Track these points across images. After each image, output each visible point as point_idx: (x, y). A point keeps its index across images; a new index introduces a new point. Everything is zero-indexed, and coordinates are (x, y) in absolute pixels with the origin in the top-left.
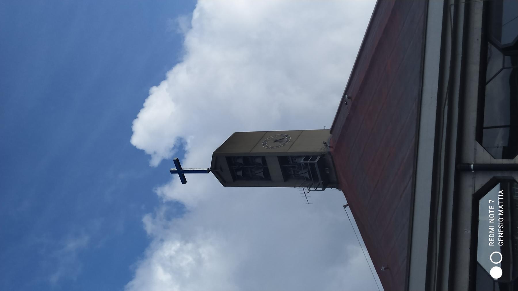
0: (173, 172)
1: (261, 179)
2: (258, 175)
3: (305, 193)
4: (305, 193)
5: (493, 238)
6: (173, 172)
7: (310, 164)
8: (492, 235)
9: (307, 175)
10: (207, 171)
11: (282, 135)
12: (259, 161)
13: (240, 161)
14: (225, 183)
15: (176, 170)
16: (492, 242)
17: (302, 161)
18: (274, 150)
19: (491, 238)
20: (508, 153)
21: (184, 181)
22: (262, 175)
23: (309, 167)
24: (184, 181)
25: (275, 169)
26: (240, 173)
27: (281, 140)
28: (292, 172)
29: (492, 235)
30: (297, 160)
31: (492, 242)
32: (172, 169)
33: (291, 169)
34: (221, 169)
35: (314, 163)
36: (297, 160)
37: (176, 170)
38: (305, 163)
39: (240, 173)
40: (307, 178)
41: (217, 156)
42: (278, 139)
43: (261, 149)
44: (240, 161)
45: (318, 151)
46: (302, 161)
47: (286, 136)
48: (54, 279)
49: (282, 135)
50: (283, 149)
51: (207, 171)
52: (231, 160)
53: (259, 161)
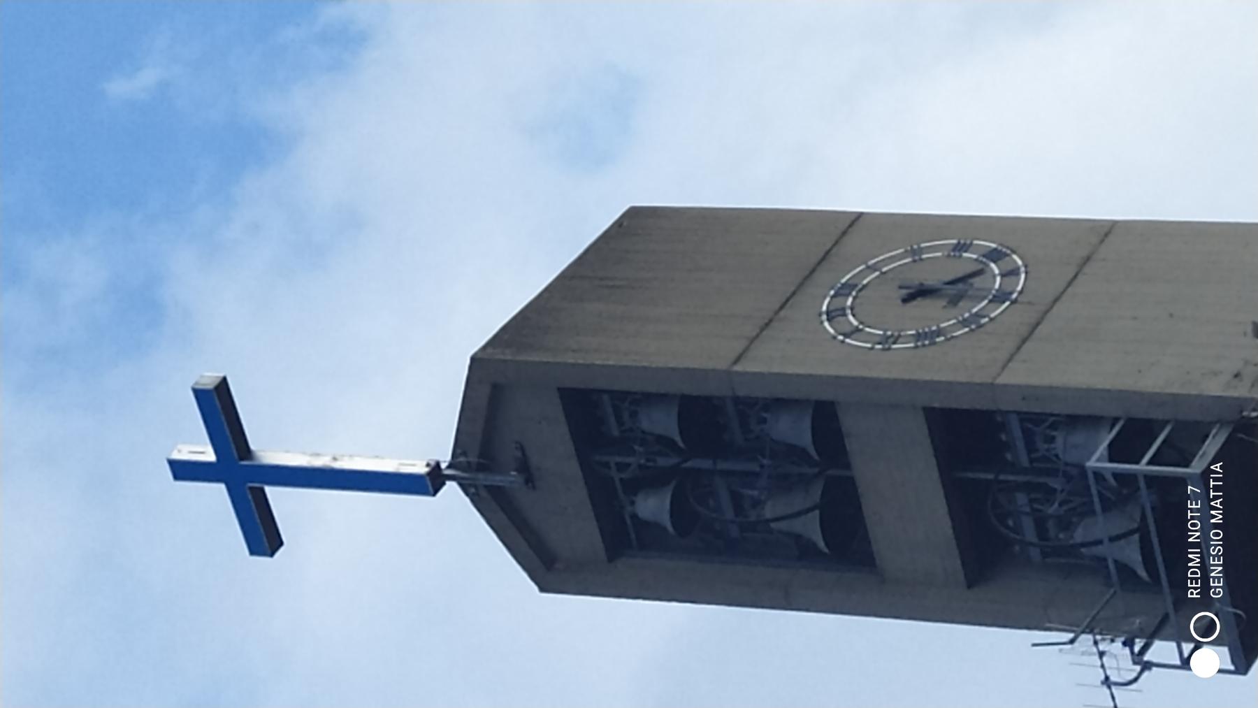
0: (183, 471)
1: (804, 552)
2: (783, 525)
3: (1107, 681)
4: (1107, 681)
5: (1196, 579)
6: (183, 471)
7: (1151, 479)
8: (1196, 573)
9: (1131, 554)
10: (432, 482)
11: (961, 247)
12: (794, 430)
13: (663, 423)
14: (550, 568)
15: (210, 456)
16: (1195, 589)
17: (1097, 461)
18: (903, 362)
19: (1192, 579)
20: (1006, 255)
21: (263, 535)
22: (811, 527)
23: (1146, 497)
24: (263, 535)
25: (906, 496)
26: (653, 507)
27: (959, 288)
28: (1028, 524)
29: (1196, 573)
30: (1064, 445)
31: (1195, 589)
32: (184, 453)
33: (1021, 499)
34: (524, 467)
35: (1182, 482)
36: (1064, 445)
37: (210, 456)
38: (1117, 476)
39: (653, 507)
40: (1125, 571)
41: (495, 383)
42: (931, 280)
43: (822, 347)
44: (663, 423)
45: (1214, 388)
46: (1097, 461)
47: (995, 255)
48: (119, 88)
49: (961, 247)
50: (964, 357)
51: (432, 482)
52: (596, 413)
53: (794, 430)
